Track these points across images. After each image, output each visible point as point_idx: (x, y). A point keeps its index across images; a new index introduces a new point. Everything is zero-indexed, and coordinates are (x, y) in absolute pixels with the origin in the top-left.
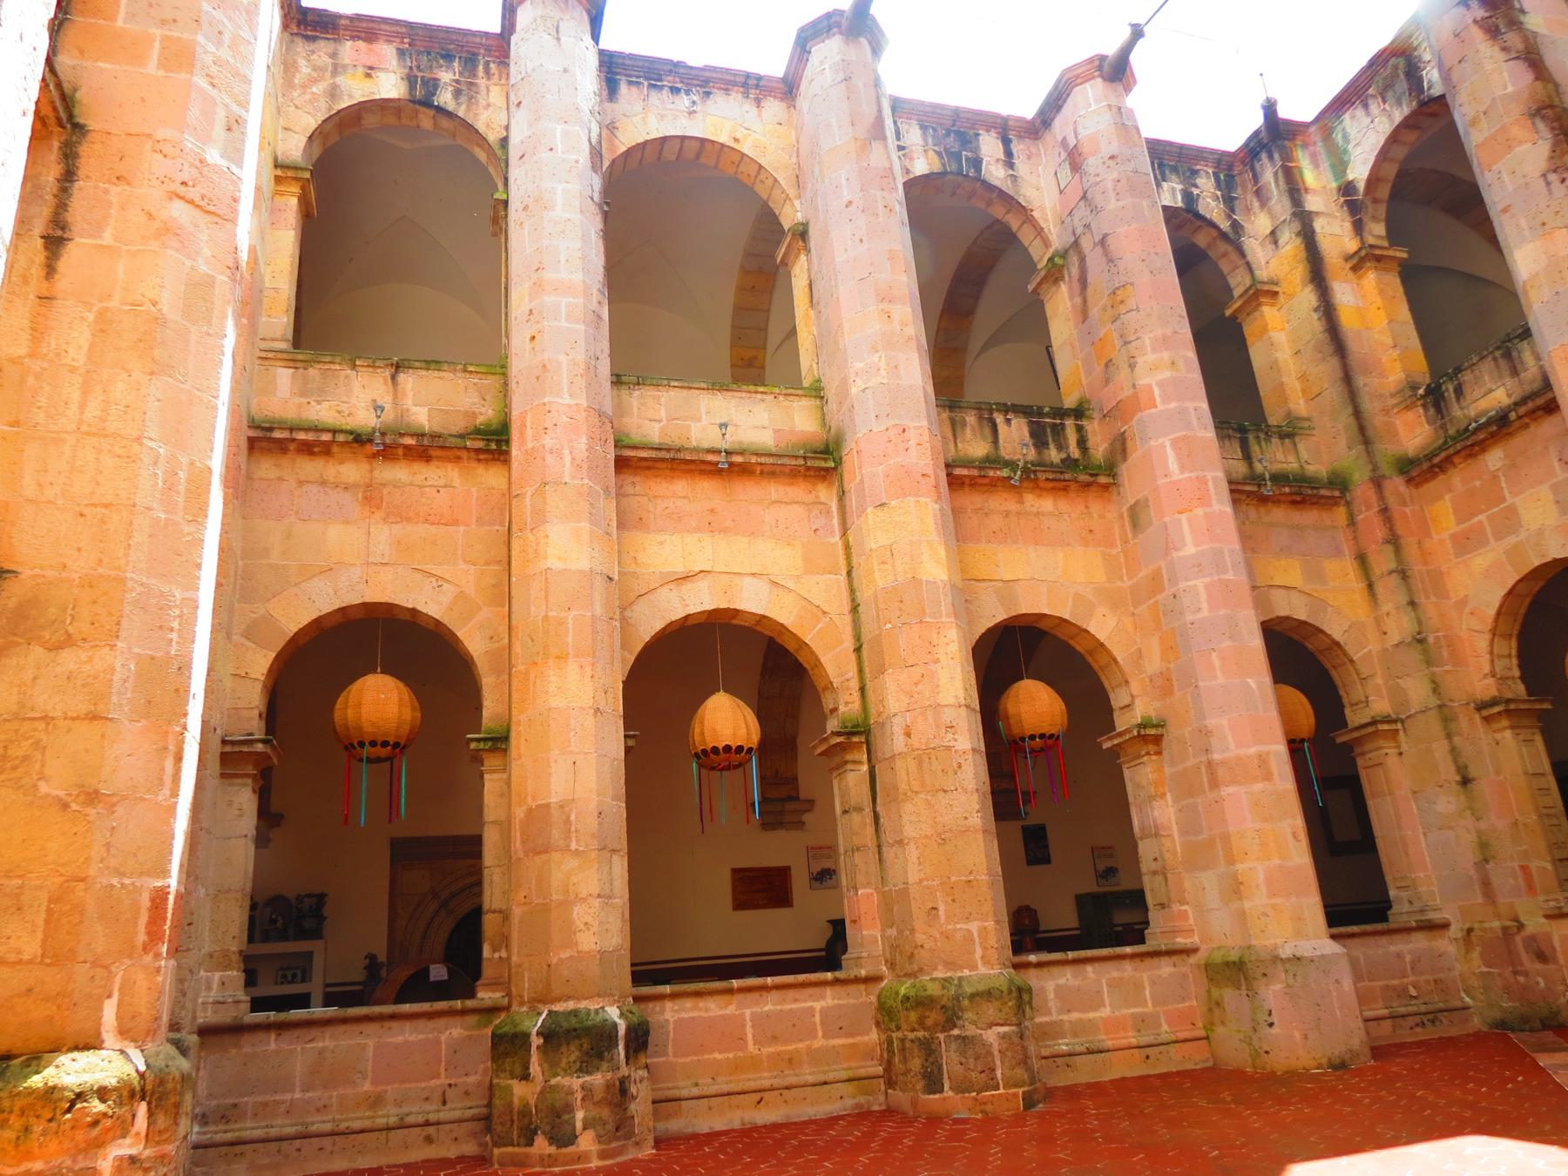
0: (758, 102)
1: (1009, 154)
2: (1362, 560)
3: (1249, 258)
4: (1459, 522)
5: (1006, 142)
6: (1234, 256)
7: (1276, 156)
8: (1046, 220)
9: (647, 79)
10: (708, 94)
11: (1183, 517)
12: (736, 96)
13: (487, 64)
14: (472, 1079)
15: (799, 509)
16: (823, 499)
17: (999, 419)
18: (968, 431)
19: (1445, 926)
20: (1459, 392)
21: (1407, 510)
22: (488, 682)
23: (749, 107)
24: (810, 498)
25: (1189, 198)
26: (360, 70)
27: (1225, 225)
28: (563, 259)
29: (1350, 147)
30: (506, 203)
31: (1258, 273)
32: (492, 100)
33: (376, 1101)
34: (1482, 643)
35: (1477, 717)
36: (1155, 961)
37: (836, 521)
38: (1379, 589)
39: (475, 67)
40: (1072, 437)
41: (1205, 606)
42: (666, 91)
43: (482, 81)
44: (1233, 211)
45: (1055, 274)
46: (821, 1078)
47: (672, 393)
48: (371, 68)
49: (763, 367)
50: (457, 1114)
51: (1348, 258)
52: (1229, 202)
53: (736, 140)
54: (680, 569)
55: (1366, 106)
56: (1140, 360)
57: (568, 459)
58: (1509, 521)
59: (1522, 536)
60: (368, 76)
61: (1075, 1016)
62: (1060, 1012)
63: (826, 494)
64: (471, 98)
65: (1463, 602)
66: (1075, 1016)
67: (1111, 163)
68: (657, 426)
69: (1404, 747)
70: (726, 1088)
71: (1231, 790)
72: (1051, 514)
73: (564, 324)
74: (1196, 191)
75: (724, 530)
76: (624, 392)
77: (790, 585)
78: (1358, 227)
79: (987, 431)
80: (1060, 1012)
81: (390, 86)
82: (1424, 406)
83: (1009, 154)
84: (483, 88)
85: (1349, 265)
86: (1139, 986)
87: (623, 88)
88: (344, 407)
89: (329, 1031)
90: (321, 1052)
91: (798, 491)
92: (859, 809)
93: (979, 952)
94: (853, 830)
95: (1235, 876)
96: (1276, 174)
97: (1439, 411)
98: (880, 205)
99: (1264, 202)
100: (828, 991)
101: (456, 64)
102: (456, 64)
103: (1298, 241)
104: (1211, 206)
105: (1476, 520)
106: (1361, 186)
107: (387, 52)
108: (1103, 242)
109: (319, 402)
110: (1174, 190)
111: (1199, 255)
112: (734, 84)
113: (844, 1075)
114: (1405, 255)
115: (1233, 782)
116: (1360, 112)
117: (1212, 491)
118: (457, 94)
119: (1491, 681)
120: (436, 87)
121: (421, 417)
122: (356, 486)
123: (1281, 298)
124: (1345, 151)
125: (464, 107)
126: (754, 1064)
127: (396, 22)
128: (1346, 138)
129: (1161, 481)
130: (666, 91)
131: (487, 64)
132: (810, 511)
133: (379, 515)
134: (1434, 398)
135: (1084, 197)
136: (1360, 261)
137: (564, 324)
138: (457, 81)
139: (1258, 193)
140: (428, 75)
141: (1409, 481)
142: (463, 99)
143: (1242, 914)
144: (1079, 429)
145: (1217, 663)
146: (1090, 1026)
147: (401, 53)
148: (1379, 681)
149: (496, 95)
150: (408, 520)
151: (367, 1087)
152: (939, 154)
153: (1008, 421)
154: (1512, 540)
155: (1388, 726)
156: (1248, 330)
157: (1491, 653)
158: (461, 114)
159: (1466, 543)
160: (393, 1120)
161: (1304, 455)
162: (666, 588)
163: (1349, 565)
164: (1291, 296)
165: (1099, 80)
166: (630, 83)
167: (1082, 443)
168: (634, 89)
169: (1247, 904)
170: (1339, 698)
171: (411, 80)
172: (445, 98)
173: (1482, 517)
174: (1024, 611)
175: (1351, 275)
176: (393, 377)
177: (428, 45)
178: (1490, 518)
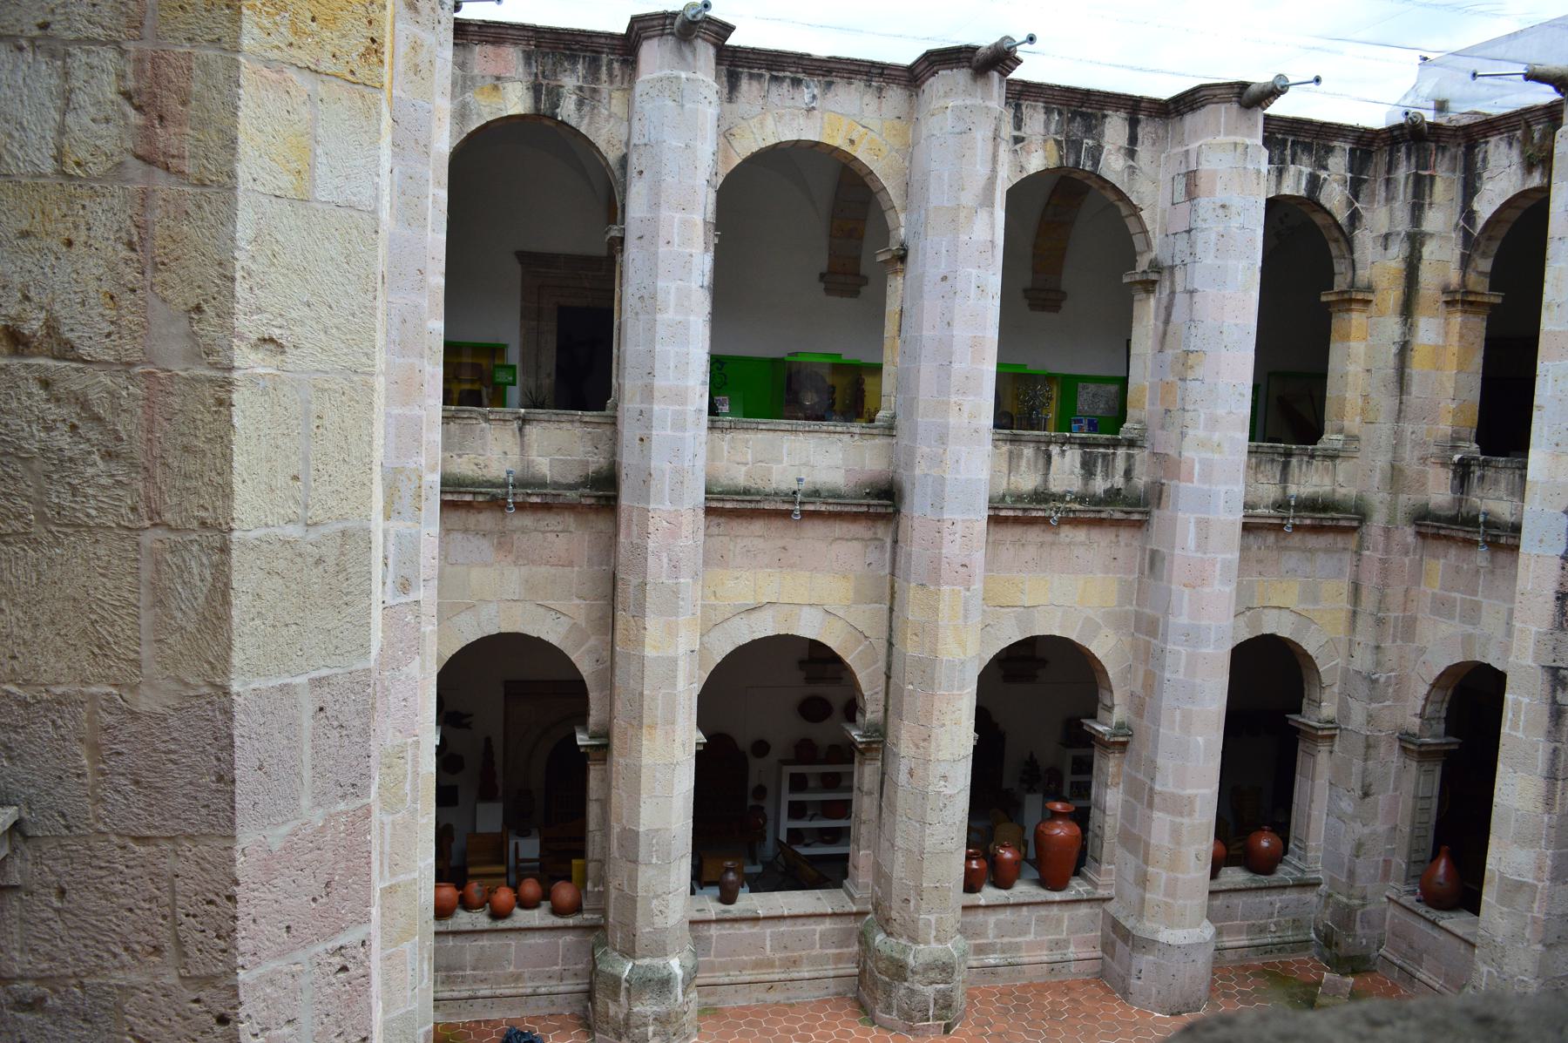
0: (880, 89)
1: (1133, 139)
2: (1356, 589)
3: (1356, 256)
4: (1443, 588)
5: (1133, 123)
6: (1344, 246)
7: (1413, 160)
8: (1154, 221)
9: (769, 69)
10: (830, 84)
11: (1187, 590)
12: (858, 84)
13: (610, 63)
14: (579, 966)
15: (857, 545)
16: (879, 535)
17: (1055, 450)
18: (1024, 463)
19: (1315, 884)
20: (1482, 478)
21: (1407, 560)
22: (593, 696)
23: (870, 98)
24: (869, 534)
25: (1314, 183)
26: (489, 81)
27: (1342, 216)
28: (672, 365)
29: (1485, 175)
30: (622, 240)
31: (1359, 272)
32: (614, 109)
33: (517, 978)
34: (1424, 689)
35: (1397, 745)
36: (1076, 906)
37: (888, 555)
38: (1360, 622)
39: (598, 68)
40: (1120, 464)
41: (1182, 670)
42: (786, 85)
43: (604, 87)
44: (1356, 197)
45: (1149, 286)
46: (816, 975)
47: (760, 435)
48: (498, 78)
49: (861, 238)
50: (570, 988)
51: (1446, 290)
52: (1356, 187)
53: (852, 142)
54: (751, 602)
55: (1510, 145)
56: (1191, 432)
57: (665, 560)
58: (1472, 614)
59: (1477, 632)
60: (496, 88)
61: (1005, 940)
62: (997, 937)
63: (882, 530)
64: (593, 108)
65: (1422, 651)
66: (1005, 940)
67: (1220, 212)
68: (744, 469)
69: (1336, 748)
70: (748, 979)
71: (1160, 814)
72: (1082, 544)
73: (669, 432)
74: (1323, 174)
75: (791, 566)
76: (717, 434)
77: (840, 614)
78: (1465, 262)
79: (1041, 462)
80: (997, 937)
81: (515, 101)
82: (1455, 472)
83: (1133, 139)
84: (605, 94)
85: (1444, 298)
86: (1059, 921)
87: (744, 84)
88: (480, 460)
89: (485, 936)
90: (482, 947)
91: (858, 529)
92: (870, 793)
93: (934, 933)
94: (864, 806)
95: (1145, 874)
96: (1407, 178)
97: (1462, 486)
98: (973, 286)
99: (1390, 199)
100: (828, 920)
101: (580, 67)
102: (580, 67)
103: (1403, 266)
104: (1334, 197)
105: (1453, 594)
106: (1480, 223)
107: (512, 57)
108: (1192, 292)
109: (460, 456)
110: (1300, 172)
111: (1302, 259)
112: (859, 72)
113: (832, 973)
114: (1499, 300)
115: (1165, 810)
116: (1503, 146)
117: (1218, 572)
118: (580, 103)
119: (1418, 721)
120: (559, 96)
121: (544, 466)
122: (491, 532)
123: (1373, 307)
124: (1480, 177)
125: (586, 121)
126: (770, 964)
127: (523, 27)
128: (1485, 160)
129: (1177, 551)
130: (786, 85)
131: (610, 63)
132: (867, 547)
133: (510, 558)
134: (1463, 473)
135: (1189, 231)
136: (1459, 299)
137: (669, 432)
138: (580, 89)
139: (1388, 182)
140: (553, 83)
141: (1421, 535)
142: (586, 109)
143: (1143, 900)
144: (1129, 457)
145: (1178, 717)
146: (1016, 947)
147: (528, 57)
148: (1336, 689)
149: (617, 103)
150: (533, 562)
151: (512, 969)
152: (1058, 143)
153: (1063, 452)
154: (1469, 629)
155: (1330, 733)
156: (1336, 324)
157: (1427, 699)
158: (583, 130)
159: (1442, 607)
160: (529, 991)
161: (1340, 479)
162: (737, 618)
163: (1345, 586)
164: (1381, 314)
165: (1236, 106)
166: (751, 76)
167: (1128, 474)
168: (755, 84)
169: (1148, 896)
170: (1303, 689)
171: (536, 89)
172: (567, 110)
173: (1458, 596)
174: (1037, 633)
175: (1442, 307)
176: (520, 430)
177: (553, 47)
178: (1463, 600)
